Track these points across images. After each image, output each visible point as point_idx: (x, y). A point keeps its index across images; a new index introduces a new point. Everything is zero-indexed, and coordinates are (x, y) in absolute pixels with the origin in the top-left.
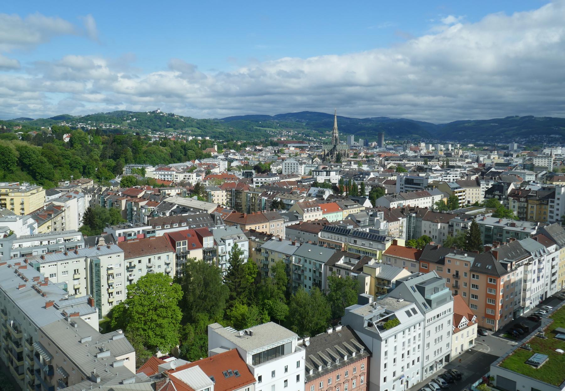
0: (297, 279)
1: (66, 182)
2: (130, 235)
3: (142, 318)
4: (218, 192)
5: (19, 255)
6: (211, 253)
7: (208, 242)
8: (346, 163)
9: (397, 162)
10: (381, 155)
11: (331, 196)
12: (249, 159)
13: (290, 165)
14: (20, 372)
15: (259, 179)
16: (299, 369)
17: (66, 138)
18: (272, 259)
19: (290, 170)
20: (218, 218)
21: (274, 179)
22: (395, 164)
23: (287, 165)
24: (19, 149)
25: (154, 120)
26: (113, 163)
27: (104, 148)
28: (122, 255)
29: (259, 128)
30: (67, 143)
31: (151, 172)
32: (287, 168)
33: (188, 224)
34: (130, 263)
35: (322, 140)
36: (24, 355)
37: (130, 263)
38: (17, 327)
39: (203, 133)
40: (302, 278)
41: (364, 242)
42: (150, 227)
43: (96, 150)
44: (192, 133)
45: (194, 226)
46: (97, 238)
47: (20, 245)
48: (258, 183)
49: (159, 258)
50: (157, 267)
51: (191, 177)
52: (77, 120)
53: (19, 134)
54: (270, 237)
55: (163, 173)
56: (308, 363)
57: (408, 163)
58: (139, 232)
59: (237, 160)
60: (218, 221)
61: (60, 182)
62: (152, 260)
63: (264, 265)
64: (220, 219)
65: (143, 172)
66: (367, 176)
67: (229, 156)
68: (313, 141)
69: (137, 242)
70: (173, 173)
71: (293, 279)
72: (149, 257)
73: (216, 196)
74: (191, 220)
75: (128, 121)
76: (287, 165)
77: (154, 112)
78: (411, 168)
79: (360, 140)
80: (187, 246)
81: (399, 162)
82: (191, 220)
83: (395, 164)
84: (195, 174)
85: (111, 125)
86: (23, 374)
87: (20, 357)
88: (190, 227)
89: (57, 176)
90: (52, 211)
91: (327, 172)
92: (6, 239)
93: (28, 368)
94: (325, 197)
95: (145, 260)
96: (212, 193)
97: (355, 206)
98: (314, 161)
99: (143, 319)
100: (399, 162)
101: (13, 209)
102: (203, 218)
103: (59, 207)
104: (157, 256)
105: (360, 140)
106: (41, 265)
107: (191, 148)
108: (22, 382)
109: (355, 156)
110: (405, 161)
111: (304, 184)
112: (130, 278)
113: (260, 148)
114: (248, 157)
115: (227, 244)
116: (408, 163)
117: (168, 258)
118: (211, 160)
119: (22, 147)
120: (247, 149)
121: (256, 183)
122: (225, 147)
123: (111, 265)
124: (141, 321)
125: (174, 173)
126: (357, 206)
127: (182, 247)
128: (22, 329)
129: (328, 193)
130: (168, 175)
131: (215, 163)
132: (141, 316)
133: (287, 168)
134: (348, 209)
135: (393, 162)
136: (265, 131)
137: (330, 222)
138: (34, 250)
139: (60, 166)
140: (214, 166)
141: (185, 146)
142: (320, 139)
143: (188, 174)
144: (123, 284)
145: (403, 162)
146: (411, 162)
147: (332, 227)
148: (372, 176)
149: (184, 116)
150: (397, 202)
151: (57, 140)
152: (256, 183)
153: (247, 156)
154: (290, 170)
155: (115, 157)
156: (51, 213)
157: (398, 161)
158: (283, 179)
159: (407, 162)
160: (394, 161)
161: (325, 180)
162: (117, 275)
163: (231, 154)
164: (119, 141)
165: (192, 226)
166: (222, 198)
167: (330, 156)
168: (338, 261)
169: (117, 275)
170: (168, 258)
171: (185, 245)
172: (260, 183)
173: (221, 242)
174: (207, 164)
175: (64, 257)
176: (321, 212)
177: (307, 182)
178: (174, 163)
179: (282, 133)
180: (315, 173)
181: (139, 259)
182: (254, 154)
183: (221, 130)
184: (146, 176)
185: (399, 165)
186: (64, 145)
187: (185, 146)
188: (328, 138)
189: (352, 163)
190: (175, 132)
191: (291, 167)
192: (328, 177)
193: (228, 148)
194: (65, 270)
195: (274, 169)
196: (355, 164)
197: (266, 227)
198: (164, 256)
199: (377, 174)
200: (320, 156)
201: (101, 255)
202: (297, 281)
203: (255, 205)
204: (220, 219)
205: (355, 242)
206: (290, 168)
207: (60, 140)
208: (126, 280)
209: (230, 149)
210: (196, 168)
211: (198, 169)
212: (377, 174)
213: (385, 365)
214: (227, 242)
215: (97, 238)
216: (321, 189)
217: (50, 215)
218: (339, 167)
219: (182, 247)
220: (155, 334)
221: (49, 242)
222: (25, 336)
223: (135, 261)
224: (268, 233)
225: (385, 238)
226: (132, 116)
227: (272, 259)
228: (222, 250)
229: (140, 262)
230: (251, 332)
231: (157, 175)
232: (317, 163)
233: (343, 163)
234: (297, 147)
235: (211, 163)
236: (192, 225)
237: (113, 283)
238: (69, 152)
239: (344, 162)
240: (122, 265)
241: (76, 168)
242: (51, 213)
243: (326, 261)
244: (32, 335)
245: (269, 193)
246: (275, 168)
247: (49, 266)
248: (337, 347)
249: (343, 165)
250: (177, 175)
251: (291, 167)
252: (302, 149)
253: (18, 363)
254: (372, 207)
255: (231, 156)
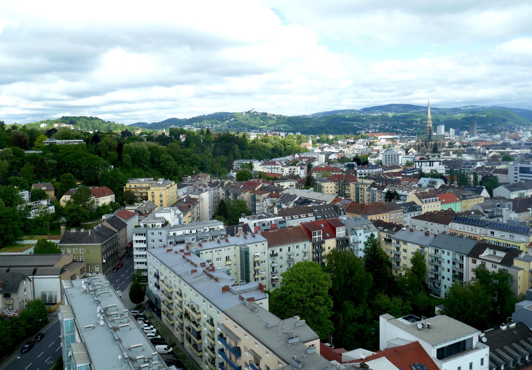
0: (434, 270)
1: (189, 177)
2: (264, 225)
3: (300, 304)
4: (327, 183)
5: (174, 243)
6: (344, 242)
7: (340, 232)
8: (445, 153)
9: (499, 150)
10: (478, 144)
11: (442, 187)
12: (344, 152)
13: (390, 157)
14: (199, 350)
15: (363, 171)
16: (483, 367)
17: (182, 138)
18: (404, 249)
19: (390, 161)
20: (341, 209)
21: (377, 171)
22: (498, 152)
23: (387, 157)
24: (150, 149)
25: (249, 119)
26: (224, 158)
27: (215, 146)
28: (266, 244)
29: (346, 122)
30: (184, 142)
31: (258, 166)
32: (388, 159)
33: (315, 215)
34: (273, 251)
35: (410, 131)
36: (202, 335)
37: (273, 251)
38: (194, 308)
39: (294, 129)
40: (439, 269)
41: (503, 233)
42: (281, 217)
43: (208, 148)
44: (284, 130)
45: (320, 217)
46: (235, 227)
47: (174, 234)
48: (362, 174)
49: (298, 247)
50: (295, 255)
51: (296, 170)
52: (184, 122)
53: (144, 137)
54: (399, 227)
55: (270, 167)
56: (491, 363)
57: (512, 152)
58: (271, 221)
59: (333, 153)
60: (342, 212)
61: (183, 176)
62: (291, 249)
63: (395, 255)
64: (343, 210)
65: (251, 166)
66: (473, 166)
67: (325, 150)
68: (401, 132)
69: (277, 232)
70: (280, 167)
71: (429, 270)
72: (289, 246)
73: (326, 188)
74: (316, 211)
75: (227, 121)
76: (387, 157)
77: (249, 112)
78: (517, 156)
79: (451, 129)
80: (321, 236)
81: (501, 150)
82: (316, 211)
83: (498, 152)
84: (299, 167)
85: (212, 125)
86: (201, 351)
87: (199, 336)
88: (316, 218)
89: (181, 172)
90: (191, 203)
91: (430, 162)
92: (163, 228)
93: (208, 347)
94: (438, 187)
95: (285, 248)
96: (323, 184)
97: (473, 196)
98: (409, 152)
99: (301, 305)
100: (501, 150)
101: (154, 201)
102: (327, 209)
103: (195, 200)
104: (296, 245)
105: (451, 129)
106: (201, 252)
107: (290, 143)
108: (200, 358)
109: (451, 146)
110: (508, 150)
111: (408, 174)
112: (273, 265)
113: (353, 141)
114: (344, 150)
115: (358, 234)
116: (512, 152)
117: (305, 248)
118: (310, 154)
119: (153, 147)
120: (340, 142)
121: (360, 175)
122: (318, 141)
123: (257, 253)
124: (300, 307)
125: (280, 166)
126: (475, 196)
127: (317, 236)
128: (201, 310)
129: (440, 183)
130: (275, 168)
131: (314, 156)
132: (299, 302)
133: (388, 159)
134: (467, 199)
135: (495, 150)
136: (353, 124)
137: (456, 212)
138: (186, 238)
139: (182, 163)
140: (314, 159)
141: (284, 141)
142: (408, 131)
143: (293, 167)
144: (267, 270)
145: (506, 151)
146: (515, 150)
147: (462, 218)
148: (479, 165)
149: (276, 114)
150: (518, 192)
151: (175, 140)
152: (360, 175)
153: (341, 148)
154: (390, 161)
155: (226, 153)
156: (190, 204)
157: (500, 149)
158: (385, 170)
159: (511, 150)
160: (495, 149)
161: (431, 170)
162: (262, 262)
163: (326, 148)
164: (227, 139)
165: (318, 217)
166: (331, 189)
167: (425, 147)
168: (482, 253)
169: (262, 262)
170: (305, 248)
171: (320, 235)
172: (363, 174)
173: (352, 232)
174: (307, 158)
175: (217, 245)
176: (439, 203)
177: (410, 173)
178: (276, 157)
179: (369, 126)
180: (417, 163)
181: (280, 247)
182: (348, 147)
183: (311, 126)
184: (254, 170)
185: (502, 153)
186: (181, 144)
187: (284, 141)
188: (415, 129)
189: (451, 152)
190: (269, 129)
191: (392, 158)
192: (431, 167)
193: (322, 142)
194: (218, 256)
195: (372, 161)
196: (454, 153)
197: (386, 217)
198: (301, 245)
199: (483, 163)
200: (415, 147)
201: (249, 244)
202: (433, 272)
203: (365, 196)
204: (343, 210)
205: (492, 233)
206: (390, 159)
207: (177, 140)
208: (269, 266)
209: (324, 142)
210: (298, 162)
211: (300, 162)
212: (483, 163)
213: (482, 364)
214: (358, 232)
215: (235, 227)
216: (432, 179)
217: (190, 207)
218: (437, 157)
219: (317, 236)
220: (313, 321)
221: (197, 231)
222: (205, 317)
223: (277, 250)
224: (398, 224)
225: (529, 229)
226: (230, 116)
227: (404, 249)
228: (354, 240)
229: (281, 250)
230: (428, 325)
231: (265, 169)
232: (413, 154)
233: (441, 153)
234: (387, 139)
235: (310, 156)
236: (318, 216)
237: (259, 269)
238: (188, 150)
239: (442, 152)
240: (266, 253)
241: (195, 164)
242: (190, 204)
243: (467, 253)
244: (213, 317)
245: (378, 184)
246: (373, 159)
247: (216, 251)
248: (514, 344)
249: (441, 155)
250: (283, 168)
251: (392, 158)
252: (393, 140)
253: (198, 342)
254: (489, 196)
255: (326, 150)
